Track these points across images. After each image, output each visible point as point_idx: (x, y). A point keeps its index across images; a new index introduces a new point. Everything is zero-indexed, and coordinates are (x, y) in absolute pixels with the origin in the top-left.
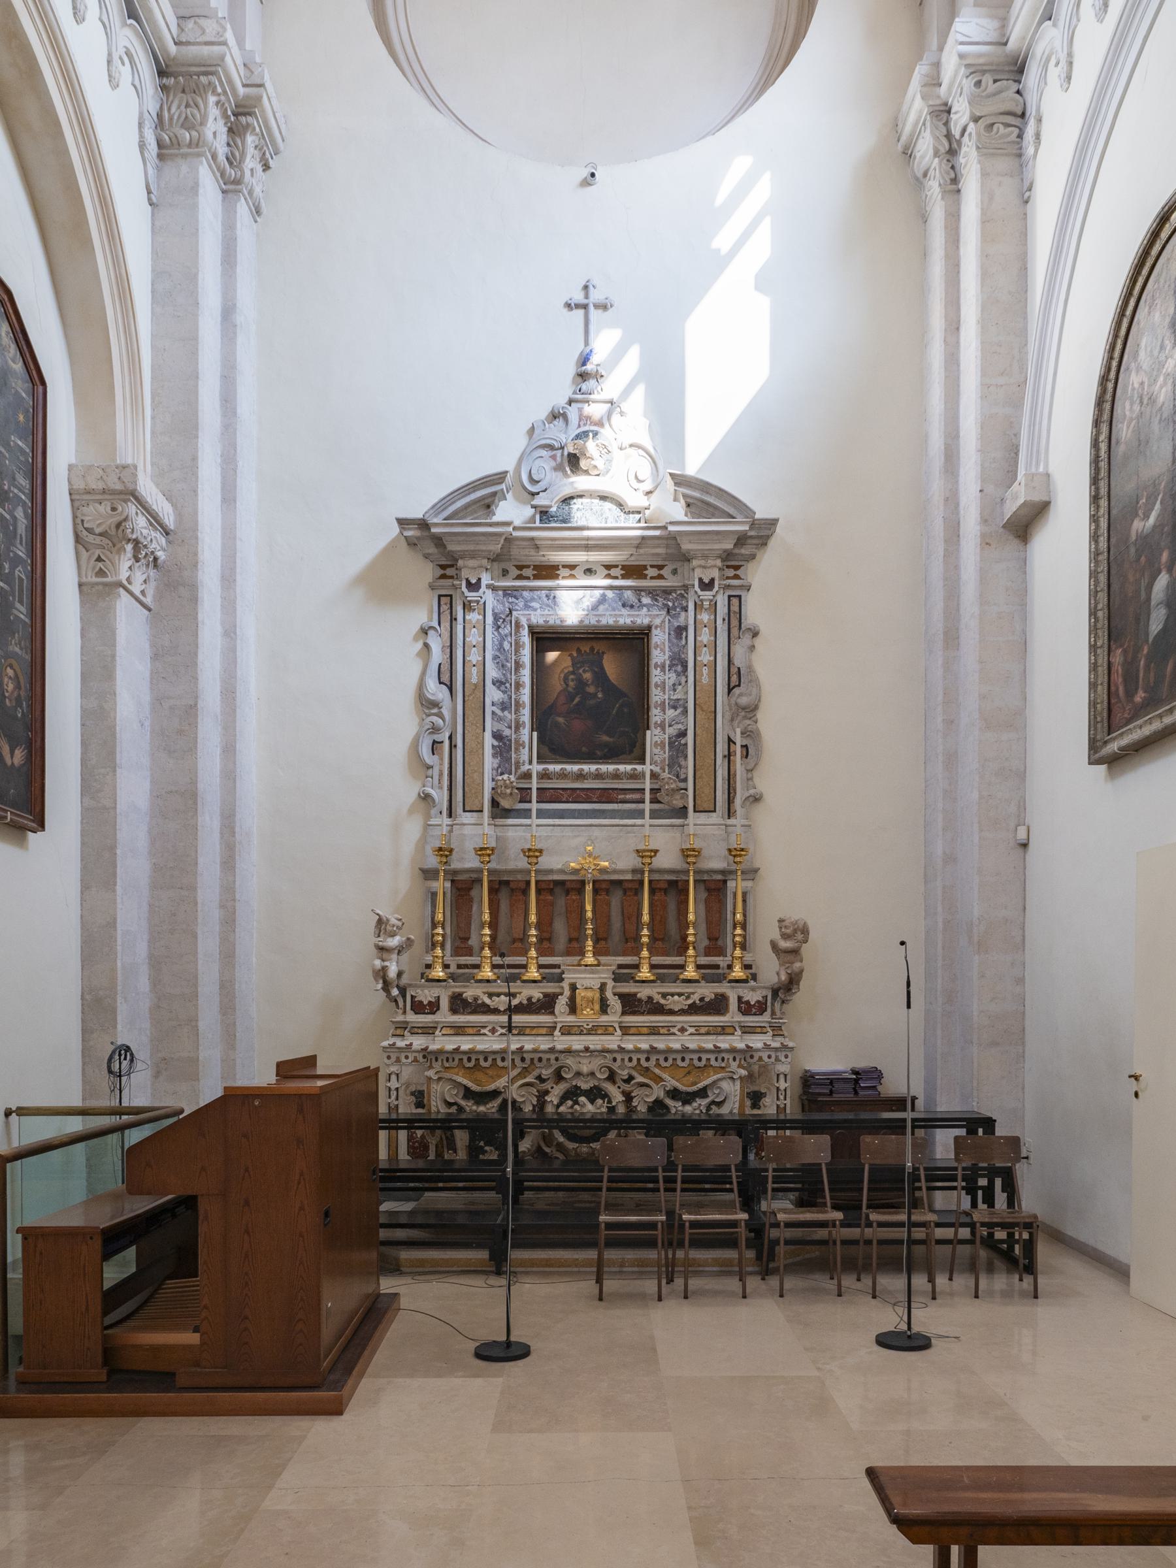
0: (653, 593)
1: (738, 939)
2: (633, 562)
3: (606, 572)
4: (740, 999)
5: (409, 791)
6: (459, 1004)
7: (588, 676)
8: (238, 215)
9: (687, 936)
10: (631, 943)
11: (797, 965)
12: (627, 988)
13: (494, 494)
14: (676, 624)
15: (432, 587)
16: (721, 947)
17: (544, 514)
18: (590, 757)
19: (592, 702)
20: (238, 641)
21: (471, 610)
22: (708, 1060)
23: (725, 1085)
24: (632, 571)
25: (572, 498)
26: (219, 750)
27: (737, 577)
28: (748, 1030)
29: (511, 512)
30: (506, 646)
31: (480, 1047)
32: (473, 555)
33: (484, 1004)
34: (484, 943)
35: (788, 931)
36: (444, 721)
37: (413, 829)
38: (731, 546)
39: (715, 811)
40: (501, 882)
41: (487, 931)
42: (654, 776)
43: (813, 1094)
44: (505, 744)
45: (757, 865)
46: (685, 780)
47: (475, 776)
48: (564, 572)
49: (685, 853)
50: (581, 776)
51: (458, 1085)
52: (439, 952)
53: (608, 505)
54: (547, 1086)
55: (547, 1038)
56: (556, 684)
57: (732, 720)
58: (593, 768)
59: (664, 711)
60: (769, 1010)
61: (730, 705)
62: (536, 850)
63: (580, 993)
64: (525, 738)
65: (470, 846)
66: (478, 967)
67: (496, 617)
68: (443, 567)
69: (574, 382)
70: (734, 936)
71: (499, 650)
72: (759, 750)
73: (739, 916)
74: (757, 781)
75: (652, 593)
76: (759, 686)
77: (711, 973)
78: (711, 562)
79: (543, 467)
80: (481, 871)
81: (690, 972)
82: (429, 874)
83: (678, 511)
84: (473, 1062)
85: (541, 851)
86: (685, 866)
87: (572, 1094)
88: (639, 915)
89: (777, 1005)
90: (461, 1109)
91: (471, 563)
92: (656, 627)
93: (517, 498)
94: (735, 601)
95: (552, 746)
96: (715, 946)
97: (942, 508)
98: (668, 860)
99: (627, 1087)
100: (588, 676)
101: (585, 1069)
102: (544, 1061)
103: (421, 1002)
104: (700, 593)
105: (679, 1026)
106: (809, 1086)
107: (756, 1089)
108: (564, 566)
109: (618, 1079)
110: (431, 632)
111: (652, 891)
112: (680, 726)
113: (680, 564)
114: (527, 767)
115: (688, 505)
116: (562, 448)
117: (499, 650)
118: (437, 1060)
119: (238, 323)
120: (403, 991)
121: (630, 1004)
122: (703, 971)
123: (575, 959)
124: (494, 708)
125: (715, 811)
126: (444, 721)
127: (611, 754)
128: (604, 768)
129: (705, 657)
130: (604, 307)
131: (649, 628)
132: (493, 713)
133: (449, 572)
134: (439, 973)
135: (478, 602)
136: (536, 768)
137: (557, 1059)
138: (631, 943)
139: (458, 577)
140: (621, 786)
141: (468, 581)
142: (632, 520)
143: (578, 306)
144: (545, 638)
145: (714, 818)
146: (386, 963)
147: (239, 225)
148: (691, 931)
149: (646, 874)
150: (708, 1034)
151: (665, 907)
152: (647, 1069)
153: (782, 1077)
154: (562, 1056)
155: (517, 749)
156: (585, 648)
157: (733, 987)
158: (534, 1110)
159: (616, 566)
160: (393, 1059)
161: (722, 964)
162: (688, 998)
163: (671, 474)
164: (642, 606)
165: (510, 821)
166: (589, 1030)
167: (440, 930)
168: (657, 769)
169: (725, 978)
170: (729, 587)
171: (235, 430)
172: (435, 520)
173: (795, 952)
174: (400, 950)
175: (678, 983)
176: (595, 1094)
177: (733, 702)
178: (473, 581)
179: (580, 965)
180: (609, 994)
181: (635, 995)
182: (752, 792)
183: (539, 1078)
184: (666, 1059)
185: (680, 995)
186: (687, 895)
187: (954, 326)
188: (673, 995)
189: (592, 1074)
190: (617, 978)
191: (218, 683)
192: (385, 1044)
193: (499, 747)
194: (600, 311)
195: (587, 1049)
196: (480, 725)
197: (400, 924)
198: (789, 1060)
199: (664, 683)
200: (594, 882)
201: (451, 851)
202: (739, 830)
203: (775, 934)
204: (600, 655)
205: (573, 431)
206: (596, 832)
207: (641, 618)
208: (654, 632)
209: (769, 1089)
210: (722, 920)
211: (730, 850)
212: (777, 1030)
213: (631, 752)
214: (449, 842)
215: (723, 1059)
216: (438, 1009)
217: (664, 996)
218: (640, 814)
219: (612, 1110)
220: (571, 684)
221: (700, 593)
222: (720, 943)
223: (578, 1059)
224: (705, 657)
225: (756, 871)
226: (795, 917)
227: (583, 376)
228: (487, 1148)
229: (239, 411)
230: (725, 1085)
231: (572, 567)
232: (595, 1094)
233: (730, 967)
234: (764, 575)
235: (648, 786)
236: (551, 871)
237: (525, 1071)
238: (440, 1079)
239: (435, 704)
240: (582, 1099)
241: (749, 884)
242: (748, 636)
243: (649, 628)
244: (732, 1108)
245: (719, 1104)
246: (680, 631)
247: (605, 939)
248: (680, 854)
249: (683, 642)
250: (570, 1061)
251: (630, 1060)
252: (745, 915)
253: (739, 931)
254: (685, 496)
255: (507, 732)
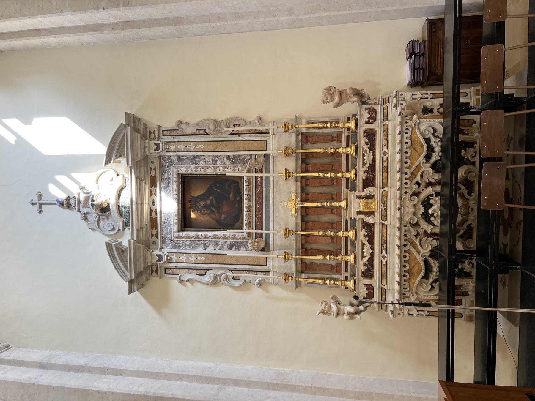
0: (162, 173)
1: (333, 125)
2: (148, 182)
3: (153, 195)
4: (366, 123)
5: (257, 291)
6: (368, 273)
7: (202, 204)
8: (5, 358)
9: (331, 153)
10: (334, 182)
11: (348, 91)
12: (359, 184)
13: (117, 248)
14: (177, 161)
15: (161, 277)
16: (337, 135)
17: (126, 225)
18: (240, 202)
19: (214, 202)
20: (184, 373)
21: (171, 259)
22: (407, 138)
23: (423, 127)
24: (153, 184)
25: (119, 211)
26: (236, 388)
27: (154, 132)
28: (386, 117)
29: (126, 239)
30: (188, 243)
31: (397, 270)
32: (145, 258)
33: (368, 261)
34: (334, 259)
35: (329, 98)
36: (223, 274)
37: (276, 291)
38: (139, 135)
39: (266, 140)
40: (302, 248)
41: (328, 257)
42: (249, 171)
43: (423, 79)
44: (234, 244)
45: (294, 117)
46: (251, 156)
47: (249, 259)
48: (154, 215)
49: (287, 155)
50: (249, 207)
51: (420, 283)
52: (339, 283)
53: (122, 195)
54: (421, 232)
55: (389, 228)
56: (206, 219)
57: (221, 133)
58: (245, 201)
59: (217, 167)
60: (373, 106)
61: (214, 134)
62: (286, 231)
63: (362, 209)
64: (231, 234)
65: (283, 264)
66: (347, 263)
67: (175, 247)
68: (152, 272)
69: (71, 209)
70: (331, 127)
71: (190, 246)
72: (239, 119)
73: (321, 125)
74: (251, 119)
75: (162, 174)
76: (205, 120)
77: (352, 139)
78: (147, 145)
79: (107, 224)
80: (296, 259)
81: (351, 150)
82: (298, 285)
83: (123, 160)
84: (406, 274)
85: (286, 229)
86: (294, 154)
87: (427, 217)
88: (320, 178)
89: (370, 102)
90: (435, 281)
91: (149, 259)
92: (178, 171)
93: (121, 237)
94: (165, 133)
95: (234, 222)
96: (337, 138)
97: (117, 31)
98: (291, 164)
99: (423, 185)
100: (202, 204)
101: (412, 210)
102: (406, 233)
103: (367, 294)
104: (161, 150)
105: (382, 155)
106: (418, 82)
107: (421, 111)
108: (151, 215)
109: (418, 191)
110: (182, 278)
111: (307, 171)
112: (225, 159)
113: (149, 159)
114: (245, 234)
115: (120, 156)
116: (99, 215)
117: (190, 246)
118: (405, 294)
119: (47, 362)
120: (361, 303)
121: (369, 182)
122: (350, 144)
123: (343, 212)
124: (217, 249)
125: (266, 140)
126: (223, 274)
127: (239, 192)
128: (245, 196)
129: (191, 147)
130: (40, 196)
131: (178, 174)
132: (219, 250)
133: (154, 269)
134: (351, 283)
135: (167, 256)
136: (245, 230)
137: (405, 226)
138: (334, 182)
139: (157, 265)
140: (254, 188)
141: (158, 261)
142: (128, 182)
143: (40, 207)
144: (185, 223)
145: (270, 141)
146: (346, 312)
147: (8, 358)
148: (328, 151)
149: (298, 175)
150: (387, 139)
151: (315, 165)
152: (412, 173)
153: (414, 97)
154: (404, 223)
155: (236, 239)
156: (189, 205)
157: (360, 127)
158: (436, 239)
159: (151, 190)
160: (400, 312)
161: (346, 134)
162: (366, 151)
163: (105, 165)
164: (168, 178)
165: (272, 243)
166: (384, 206)
167: (328, 282)
168: (246, 170)
169: (355, 131)
170: (159, 136)
171: (91, 367)
172: (129, 276)
173: (341, 93)
174: (338, 303)
175: (357, 157)
176: (427, 204)
177: (212, 133)
178: (158, 258)
179: (346, 210)
180: (363, 194)
181: (363, 180)
182: (256, 121)
183: (416, 236)
184: (406, 163)
185: (364, 156)
186: (309, 153)
187: (37, 32)
188: (364, 160)
189: (415, 206)
190: (354, 189)
191: (204, 385)
192: (391, 316)
193: (235, 247)
194: (42, 198)
195: (399, 209)
196: (225, 256)
197: (324, 303)
198: (403, 93)
199: (204, 167)
200: (302, 201)
201: (286, 274)
202: (275, 127)
203: (331, 104)
204: (192, 197)
205: (92, 210)
206: (277, 200)
207: (174, 178)
208: (180, 172)
209: (421, 104)
210: (323, 135)
211: (286, 132)
212: (386, 101)
213: (238, 182)
214: (282, 274)
215: (407, 129)
216: (371, 285)
217: (364, 164)
218: (268, 178)
219: (437, 194)
220: (206, 211)
221: (161, 150)
222: (335, 135)
223: (405, 214)
224: (191, 147)
225: (296, 117)
226: (321, 95)
227: (69, 206)
228: (460, 267)
229: (83, 365)
230: (423, 127)
231: (151, 211)
232: (427, 204)
233: (348, 129)
234: (153, 119)
235: (255, 175)
236: (297, 223)
237: (413, 244)
238: (416, 293)
239: (215, 277)
240: (430, 211)
241: (303, 121)
242: (181, 126)
243: (178, 174)
244: (437, 123)
245: (435, 130)
246: (179, 159)
247: (332, 195)
248: (287, 158)
249: (185, 157)
250: (407, 219)
251: (406, 183)
252: (320, 122)
253: (329, 125)
254: (116, 158)
255: (228, 243)
